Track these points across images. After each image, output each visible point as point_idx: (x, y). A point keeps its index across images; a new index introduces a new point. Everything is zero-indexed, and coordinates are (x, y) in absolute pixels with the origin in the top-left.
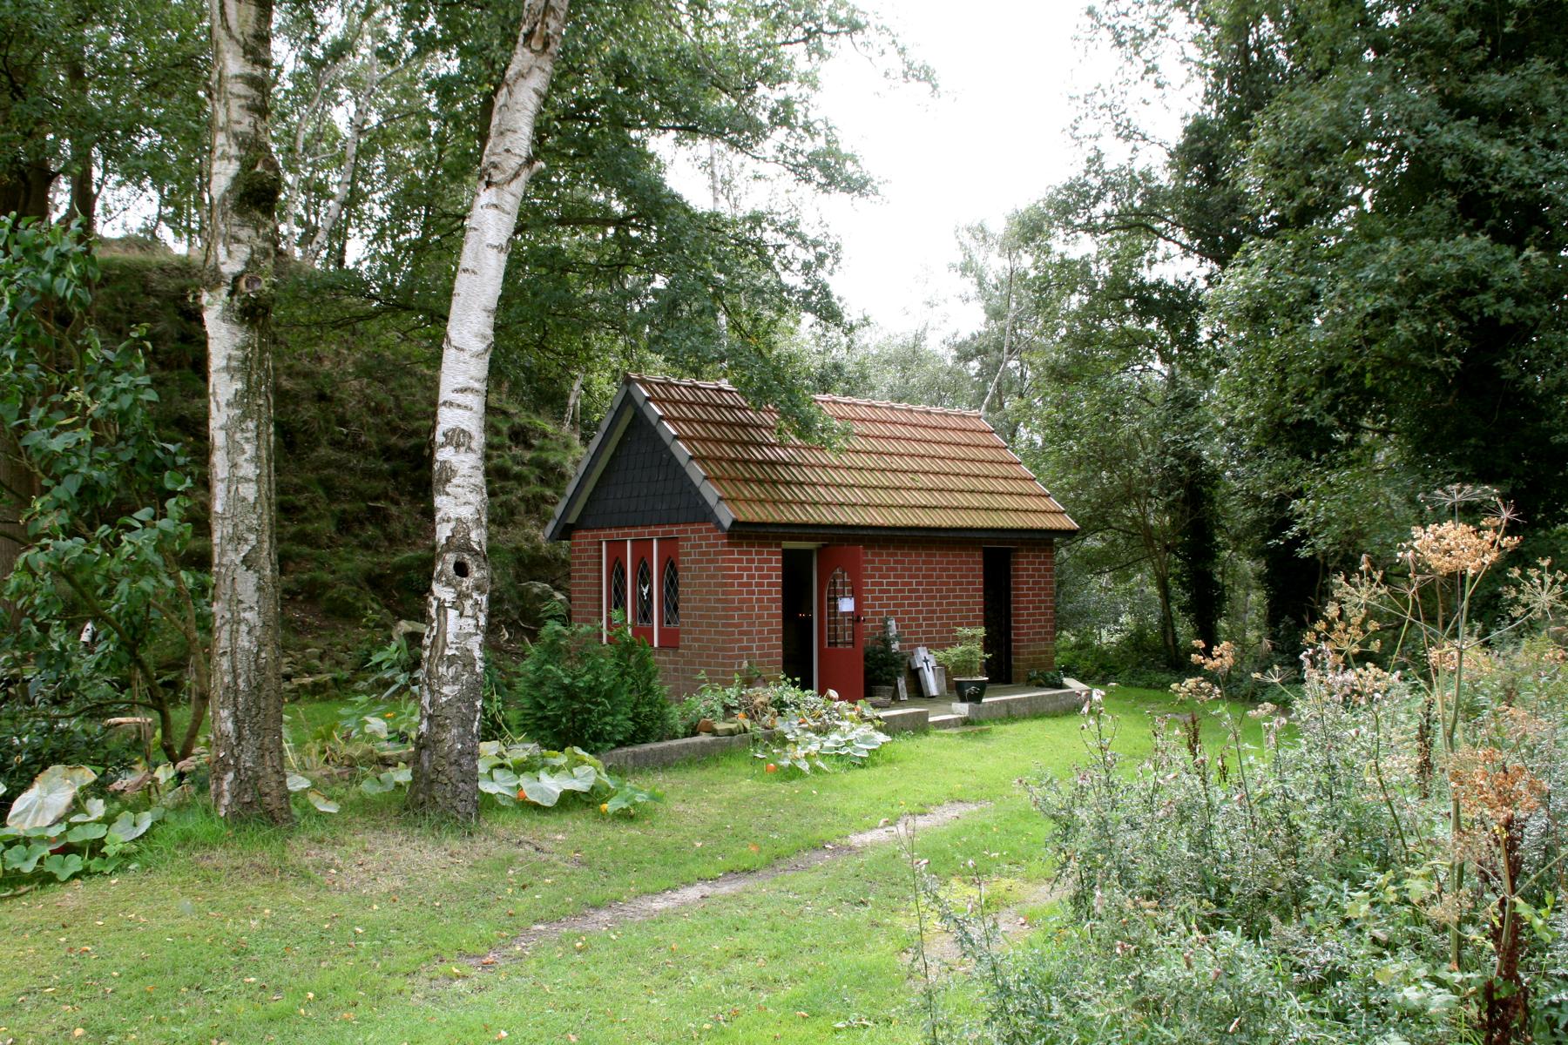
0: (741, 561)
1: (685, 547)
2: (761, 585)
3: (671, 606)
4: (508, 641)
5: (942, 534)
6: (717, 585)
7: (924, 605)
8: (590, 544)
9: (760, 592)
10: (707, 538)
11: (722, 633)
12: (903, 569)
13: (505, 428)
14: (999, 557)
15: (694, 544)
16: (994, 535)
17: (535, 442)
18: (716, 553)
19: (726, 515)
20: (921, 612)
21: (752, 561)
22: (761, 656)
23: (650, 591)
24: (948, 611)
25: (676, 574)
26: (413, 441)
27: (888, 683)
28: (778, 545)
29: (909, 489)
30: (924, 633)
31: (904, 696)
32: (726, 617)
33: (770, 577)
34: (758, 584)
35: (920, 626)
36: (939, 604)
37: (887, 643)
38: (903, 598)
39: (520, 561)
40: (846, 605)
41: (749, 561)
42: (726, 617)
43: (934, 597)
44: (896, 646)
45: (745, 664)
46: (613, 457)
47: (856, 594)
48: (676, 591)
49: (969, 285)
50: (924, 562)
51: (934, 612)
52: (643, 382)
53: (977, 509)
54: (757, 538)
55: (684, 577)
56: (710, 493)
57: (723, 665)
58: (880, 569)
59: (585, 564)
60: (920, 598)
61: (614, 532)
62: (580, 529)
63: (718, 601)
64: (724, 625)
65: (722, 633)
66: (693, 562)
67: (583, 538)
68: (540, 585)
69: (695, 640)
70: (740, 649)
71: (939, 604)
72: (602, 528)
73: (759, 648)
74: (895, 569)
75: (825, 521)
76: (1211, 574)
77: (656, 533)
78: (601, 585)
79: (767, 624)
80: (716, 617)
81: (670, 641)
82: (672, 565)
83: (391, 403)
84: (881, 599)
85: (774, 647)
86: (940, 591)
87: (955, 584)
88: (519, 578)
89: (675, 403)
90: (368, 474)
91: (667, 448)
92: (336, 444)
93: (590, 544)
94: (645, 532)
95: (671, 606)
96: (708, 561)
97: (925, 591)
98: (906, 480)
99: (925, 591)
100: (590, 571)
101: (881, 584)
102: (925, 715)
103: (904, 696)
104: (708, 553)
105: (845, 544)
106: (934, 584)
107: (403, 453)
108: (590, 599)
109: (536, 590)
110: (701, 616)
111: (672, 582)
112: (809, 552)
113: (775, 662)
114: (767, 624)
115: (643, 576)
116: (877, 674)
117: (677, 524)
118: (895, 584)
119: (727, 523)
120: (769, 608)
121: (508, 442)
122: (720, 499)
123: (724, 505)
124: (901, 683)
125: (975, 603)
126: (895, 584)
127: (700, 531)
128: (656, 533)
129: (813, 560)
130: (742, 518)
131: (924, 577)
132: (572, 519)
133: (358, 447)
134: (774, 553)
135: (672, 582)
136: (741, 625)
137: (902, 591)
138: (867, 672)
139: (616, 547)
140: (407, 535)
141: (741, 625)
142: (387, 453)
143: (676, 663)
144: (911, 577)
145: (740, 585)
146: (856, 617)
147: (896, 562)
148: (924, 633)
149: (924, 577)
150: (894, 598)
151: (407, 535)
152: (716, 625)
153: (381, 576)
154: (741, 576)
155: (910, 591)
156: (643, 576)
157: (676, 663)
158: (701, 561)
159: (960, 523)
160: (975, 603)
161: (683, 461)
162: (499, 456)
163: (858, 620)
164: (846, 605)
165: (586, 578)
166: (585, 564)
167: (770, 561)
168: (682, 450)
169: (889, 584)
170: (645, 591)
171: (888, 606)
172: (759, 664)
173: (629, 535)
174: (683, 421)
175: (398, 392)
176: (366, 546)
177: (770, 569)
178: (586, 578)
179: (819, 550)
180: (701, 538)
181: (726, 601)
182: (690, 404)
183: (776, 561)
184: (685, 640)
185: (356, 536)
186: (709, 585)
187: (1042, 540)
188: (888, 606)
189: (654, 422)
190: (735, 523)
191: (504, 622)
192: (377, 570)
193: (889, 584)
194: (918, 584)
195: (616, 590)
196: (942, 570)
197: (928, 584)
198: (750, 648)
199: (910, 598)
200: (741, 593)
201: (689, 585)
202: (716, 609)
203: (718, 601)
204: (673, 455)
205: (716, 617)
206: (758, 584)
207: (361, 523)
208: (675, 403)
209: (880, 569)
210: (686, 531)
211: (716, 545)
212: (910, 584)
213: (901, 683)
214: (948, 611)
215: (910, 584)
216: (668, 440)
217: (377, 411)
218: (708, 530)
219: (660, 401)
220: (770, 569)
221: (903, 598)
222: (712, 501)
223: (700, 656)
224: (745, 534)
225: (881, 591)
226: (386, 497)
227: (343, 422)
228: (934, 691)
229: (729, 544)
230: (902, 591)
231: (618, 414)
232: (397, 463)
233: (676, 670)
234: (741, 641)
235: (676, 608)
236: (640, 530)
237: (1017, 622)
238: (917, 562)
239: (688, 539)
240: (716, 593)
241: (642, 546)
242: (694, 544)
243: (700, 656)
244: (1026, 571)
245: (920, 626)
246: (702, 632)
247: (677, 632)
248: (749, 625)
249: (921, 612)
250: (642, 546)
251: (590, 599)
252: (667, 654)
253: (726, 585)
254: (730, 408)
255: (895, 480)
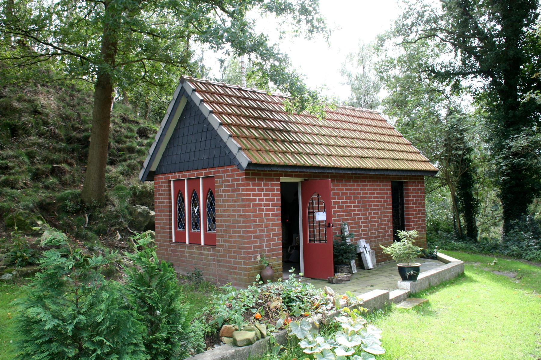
0: (254, 190)
1: (219, 182)
2: (268, 205)
3: (212, 220)
4: (121, 240)
5: (372, 173)
6: (239, 206)
7: (362, 214)
8: (164, 182)
9: (267, 210)
10: (233, 176)
11: (242, 237)
12: (350, 194)
13: (135, 129)
14: (400, 185)
15: (225, 180)
16: (398, 174)
17: (150, 135)
18: (238, 185)
19: (244, 159)
20: (360, 219)
21: (262, 190)
22: (268, 251)
23: (199, 210)
24: (374, 218)
25: (214, 199)
26: (84, 134)
27: (346, 264)
28: (278, 180)
29: (351, 147)
30: (363, 231)
31: (355, 270)
32: (246, 227)
33: (273, 200)
34: (266, 205)
35: (360, 227)
36: (370, 214)
37: (344, 238)
38: (351, 211)
39: (134, 194)
40: (321, 216)
41: (259, 190)
42: (246, 227)
43: (367, 210)
44: (348, 241)
45: (259, 258)
46: (176, 130)
47: (327, 209)
48: (214, 210)
49: (345, 79)
50: (362, 190)
51: (367, 218)
52: (191, 81)
53: (388, 159)
54: (265, 175)
55: (218, 201)
56: (233, 145)
57: (244, 258)
58: (338, 194)
59: (162, 194)
60: (360, 210)
61: (177, 174)
62: (158, 174)
63: (240, 216)
64: (244, 232)
65: (242, 237)
66: (224, 191)
67: (161, 179)
68: (142, 207)
69: (226, 241)
70: (255, 247)
71: (370, 214)
72: (170, 173)
73: (267, 246)
74: (346, 194)
75: (307, 164)
76: (472, 195)
77: (201, 174)
78: (170, 207)
79: (272, 230)
80: (239, 227)
81: (211, 242)
82: (211, 194)
83: (75, 116)
84: (339, 212)
85: (276, 245)
86: (370, 206)
87: (378, 201)
88: (133, 203)
89: (212, 94)
90: (56, 150)
91: (206, 119)
92: (41, 135)
93: (164, 182)
94: (194, 174)
95: (212, 220)
96: (234, 191)
97: (362, 206)
98: (349, 142)
99: (362, 206)
100: (164, 198)
101: (339, 203)
102: (387, 295)
103: (355, 270)
104: (233, 185)
105: (318, 178)
106: (367, 202)
107: (79, 140)
108: (165, 215)
109: (139, 210)
110: (229, 226)
111: (211, 204)
112: (296, 184)
113: (277, 255)
114: (272, 230)
115: (194, 201)
116: (340, 261)
117: (213, 167)
118: (346, 202)
119: (244, 165)
120: (273, 220)
121: (136, 135)
122: (240, 149)
123: (242, 152)
124: (353, 263)
125: (388, 213)
126: (346, 202)
127: (227, 171)
128: (201, 174)
129: (299, 190)
130: (254, 161)
131: (362, 198)
132: (154, 168)
133: (54, 137)
134: (276, 185)
135: (211, 204)
136: (255, 232)
137: (350, 207)
138: (335, 256)
139: (179, 183)
140: (74, 181)
141: (255, 232)
142: (69, 140)
143: (214, 255)
144: (355, 198)
145: (254, 205)
146: (328, 224)
147: (346, 189)
148: (363, 231)
149: (362, 198)
150: (346, 211)
151: (74, 181)
152: (239, 232)
153: (49, 204)
154: (255, 200)
155: (355, 206)
156: (194, 201)
157: (214, 255)
158: (228, 191)
159: (381, 166)
160: (388, 213)
161: (215, 126)
162: (130, 142)
163: (329, 226)
164: (321, 216)
165: (162, 203)
166: (162, 194)
167: (273, 190)
168: (215, 120)
169: (343, 203)
170: (196, 210)
171: (343, 216)
172: (268, 256)
173: (186, 176)
174: (216, 103)
175: (80, 111)
176: (47, 188)
177: (273, 195)
178: (162, 203)
179: (302, 182)
180: (228, 176)
181: (245, 216)
182: (221, 95)
183: (277, 190)
184: (219, 241)
185: (43, 183)
186: (339, 203)
187: (418, 176)
188: (343, 216)
189: (198, 103)
190: (250, 164)
191: (119, 229)
192: (48, 201)
193: (343, 203)
194: (359, 202)
195: (179, 210)
196: (371, 194)
197: (364, 202)
198: (261, 246)
199: (354, 211)
200: (255, 211)
201: (221, 206)
202: (238, 222)
203: (240, 216)
204: (210, 124)
205: (239, 227)
206: (266, 205)
207: (47, 176)
208: (212, 94)
209: (338, 194)
210: (219, 172)
211: (238, 180)
212: (354, 202)
213: (353, 263)
214: (374, 218)
215: (354, 202)
216: (206, 114)
217: (66, 118)
218: (232, 171)
219: (202, 92)
220: (273, 195)
221: (351, 211)
222: (234, 151)
223: (229, 252)
224: (256, 171)
225: (339, 207)
226: (66, 162)
227: (46, 124)
228: (371, 266)
229: (247, 179)
230: (350, 207)
231: (177, 101)
232: (75, 145)
233: (214, 260)
234: (255, 242)
235: (214, 221)
236: (191, 172)
237: (408, 222)
238: (357, 189)
239: (221, 177)
240: (239, 211)
241: (193, 182)
242: (225, 180)
243: (229, 252)
244: (412, 192)
245: (360, 227)
246: (230, 237)
247: (214, 236)
248: (261, 231)
249: (360, 219)
250: (193, 182)
251: (165, 215)
252: (208, 250)
253: (244, 206)
254: (246, 99)
255: (344, 142)
